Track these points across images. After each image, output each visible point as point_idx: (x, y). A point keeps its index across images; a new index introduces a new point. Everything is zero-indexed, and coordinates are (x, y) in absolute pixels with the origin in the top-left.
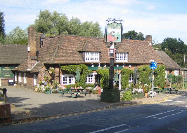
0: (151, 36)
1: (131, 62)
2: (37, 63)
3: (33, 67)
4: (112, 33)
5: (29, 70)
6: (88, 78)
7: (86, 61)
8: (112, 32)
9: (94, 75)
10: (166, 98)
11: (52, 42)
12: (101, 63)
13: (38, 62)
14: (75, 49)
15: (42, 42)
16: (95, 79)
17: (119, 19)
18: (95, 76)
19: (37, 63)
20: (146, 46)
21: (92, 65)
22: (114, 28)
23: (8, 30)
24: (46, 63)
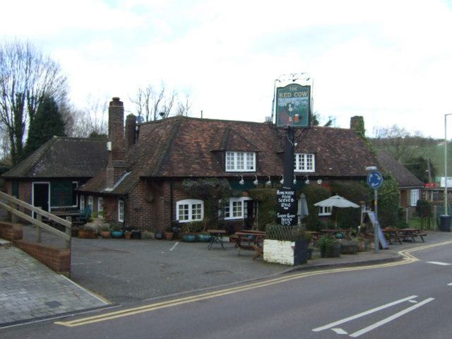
0: (361, 118)
1: (323, 173)
2: (125, 175)
3: (118, 184)
4: (287, 107)
5: (109, 190)
6: (231, 207)
7: (227, 170)
8: (288, 105)
9: (245, 201)
10: (407, 252)
11: (158, 131)
12: (259, 174)
13: (128, 174)
14: (203, 146)
15: (138, 132)
16: (246, 209)
17: (303, 76)
18: (246, 203)
19: (125, 175)
20: (352, 139)
21: (255, 180)
22: (293, 96)
23: (293, 244)
24: (143, 174)
